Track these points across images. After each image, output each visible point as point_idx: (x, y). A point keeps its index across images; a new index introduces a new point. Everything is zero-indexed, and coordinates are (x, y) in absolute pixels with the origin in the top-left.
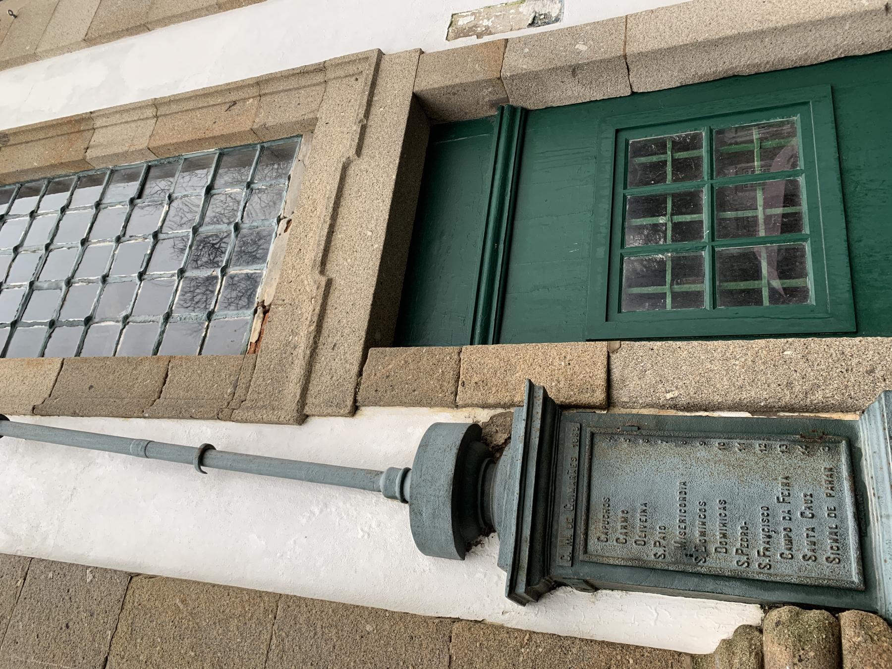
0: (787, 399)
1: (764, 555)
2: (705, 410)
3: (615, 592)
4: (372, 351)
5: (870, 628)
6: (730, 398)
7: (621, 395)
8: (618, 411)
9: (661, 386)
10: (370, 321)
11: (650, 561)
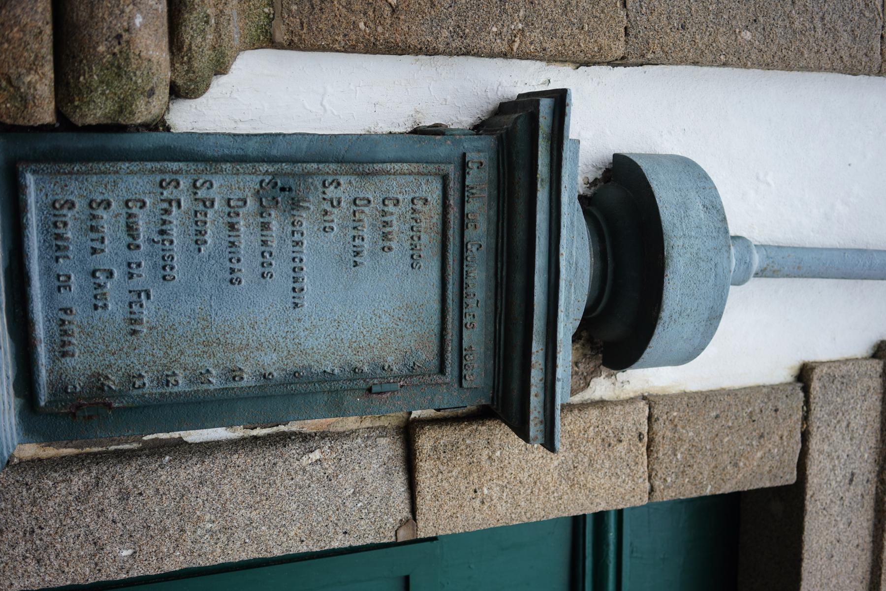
0: (127, 473)
1: (170, 202)
2: (256, 438)
3: (386, 130)
4: (791, 478)
5: (12, 98)
6: (220, 461)
7: (388, 448)
8: (393, 419)
9: (330, 471)
10: (800, 530)
11: (347, 174)
